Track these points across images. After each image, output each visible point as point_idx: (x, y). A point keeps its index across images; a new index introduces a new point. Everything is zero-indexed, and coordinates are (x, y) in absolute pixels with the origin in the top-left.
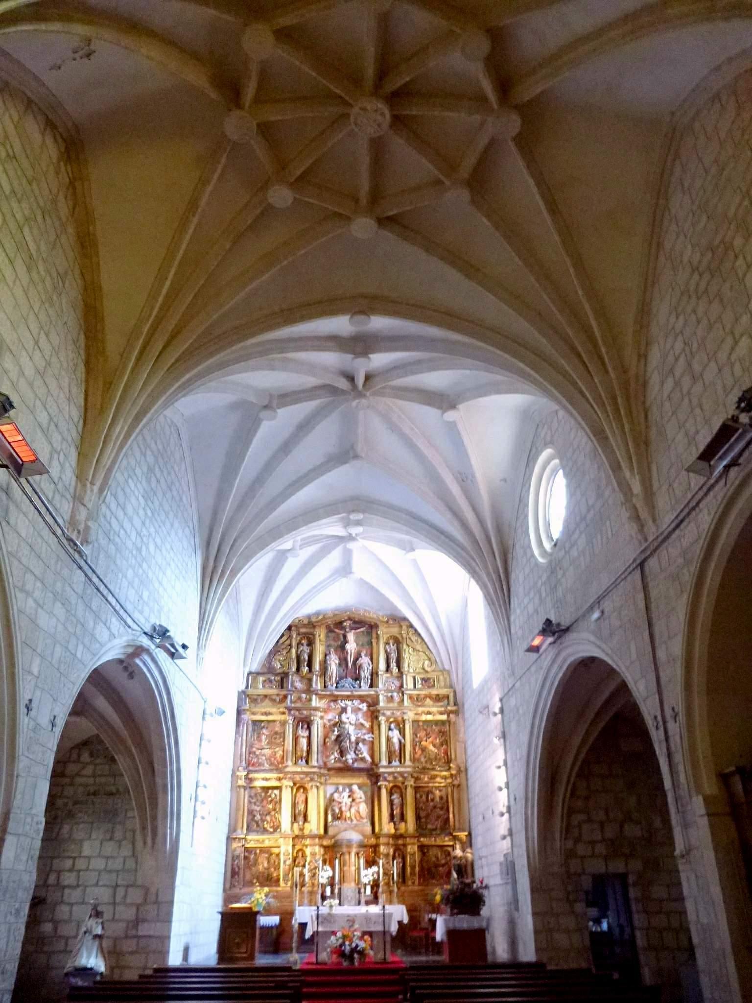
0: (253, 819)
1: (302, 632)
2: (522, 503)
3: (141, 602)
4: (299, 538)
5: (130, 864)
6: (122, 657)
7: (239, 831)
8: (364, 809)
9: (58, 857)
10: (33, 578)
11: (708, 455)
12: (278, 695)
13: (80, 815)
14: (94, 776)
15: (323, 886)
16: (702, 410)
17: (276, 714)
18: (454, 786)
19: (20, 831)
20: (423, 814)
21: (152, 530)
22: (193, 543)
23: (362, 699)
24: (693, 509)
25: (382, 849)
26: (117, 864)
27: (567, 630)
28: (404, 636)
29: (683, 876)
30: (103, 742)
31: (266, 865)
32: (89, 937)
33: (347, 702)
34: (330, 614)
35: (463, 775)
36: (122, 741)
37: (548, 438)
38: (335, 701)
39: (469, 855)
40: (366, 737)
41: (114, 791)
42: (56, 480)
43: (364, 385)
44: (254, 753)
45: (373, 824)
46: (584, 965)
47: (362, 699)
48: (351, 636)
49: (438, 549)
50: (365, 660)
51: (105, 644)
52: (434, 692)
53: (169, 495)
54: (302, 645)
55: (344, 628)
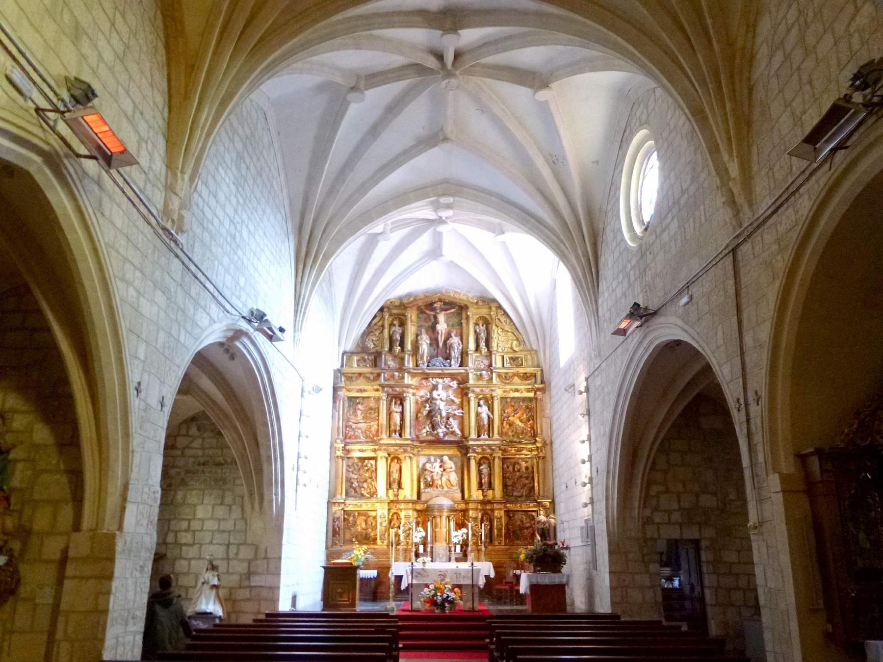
0: (351, 486)
1: (394, 313)
2: (614, 185)
3: (238, 287)
4: (390, 222)
5: (240, 525)
6: (221, 340)
7: (339, 496)
8: (454, 477)
9: (175, 518)
10: (132, 267)
11: (813, 138)
12: (371, 373)
13: (192, 483)
14: (203, 448)
15: (417, 545)
16: (811, 86)
17: (370, 391)
18: (539, 457)
19: (139, 500)
20: (509, 482)
21: (245, 217)
22: (285, 228)
23: (453, 377)
24: (793, 193)
25: (471, 513)
26: (228, 525)
27: (655, 313)
28: (494, 317)
29: (755, 545)
30: (209, 417)
31: (364, 526)
32: (206, 587)
33: (438, 380)
34: (422, 296)
35: (548, 447)
36: (227, 416)
37: (644, 118)
38: (426, 379)
39: (552, 520)
40: (456, 412)
41: (223, 462)
42: (146, 170)
43: (453, 64)
44: (351, 427)
45: (463, 492)
46: (656, 618)
47: (453, 377)
48: (441, 318)
49: (528, 232)
50: (455, 340)
51: (206, 328)
52: (522, 370)
53: (259, 181)
54: (394, 325)
55: (434, 310)
